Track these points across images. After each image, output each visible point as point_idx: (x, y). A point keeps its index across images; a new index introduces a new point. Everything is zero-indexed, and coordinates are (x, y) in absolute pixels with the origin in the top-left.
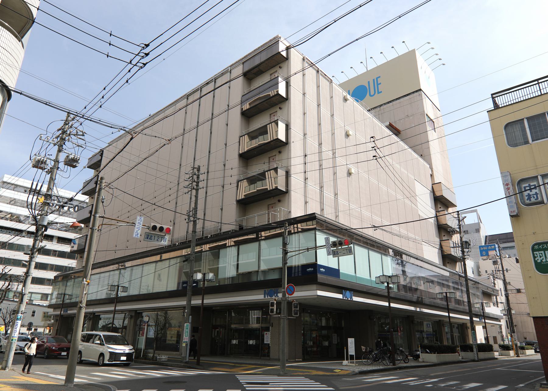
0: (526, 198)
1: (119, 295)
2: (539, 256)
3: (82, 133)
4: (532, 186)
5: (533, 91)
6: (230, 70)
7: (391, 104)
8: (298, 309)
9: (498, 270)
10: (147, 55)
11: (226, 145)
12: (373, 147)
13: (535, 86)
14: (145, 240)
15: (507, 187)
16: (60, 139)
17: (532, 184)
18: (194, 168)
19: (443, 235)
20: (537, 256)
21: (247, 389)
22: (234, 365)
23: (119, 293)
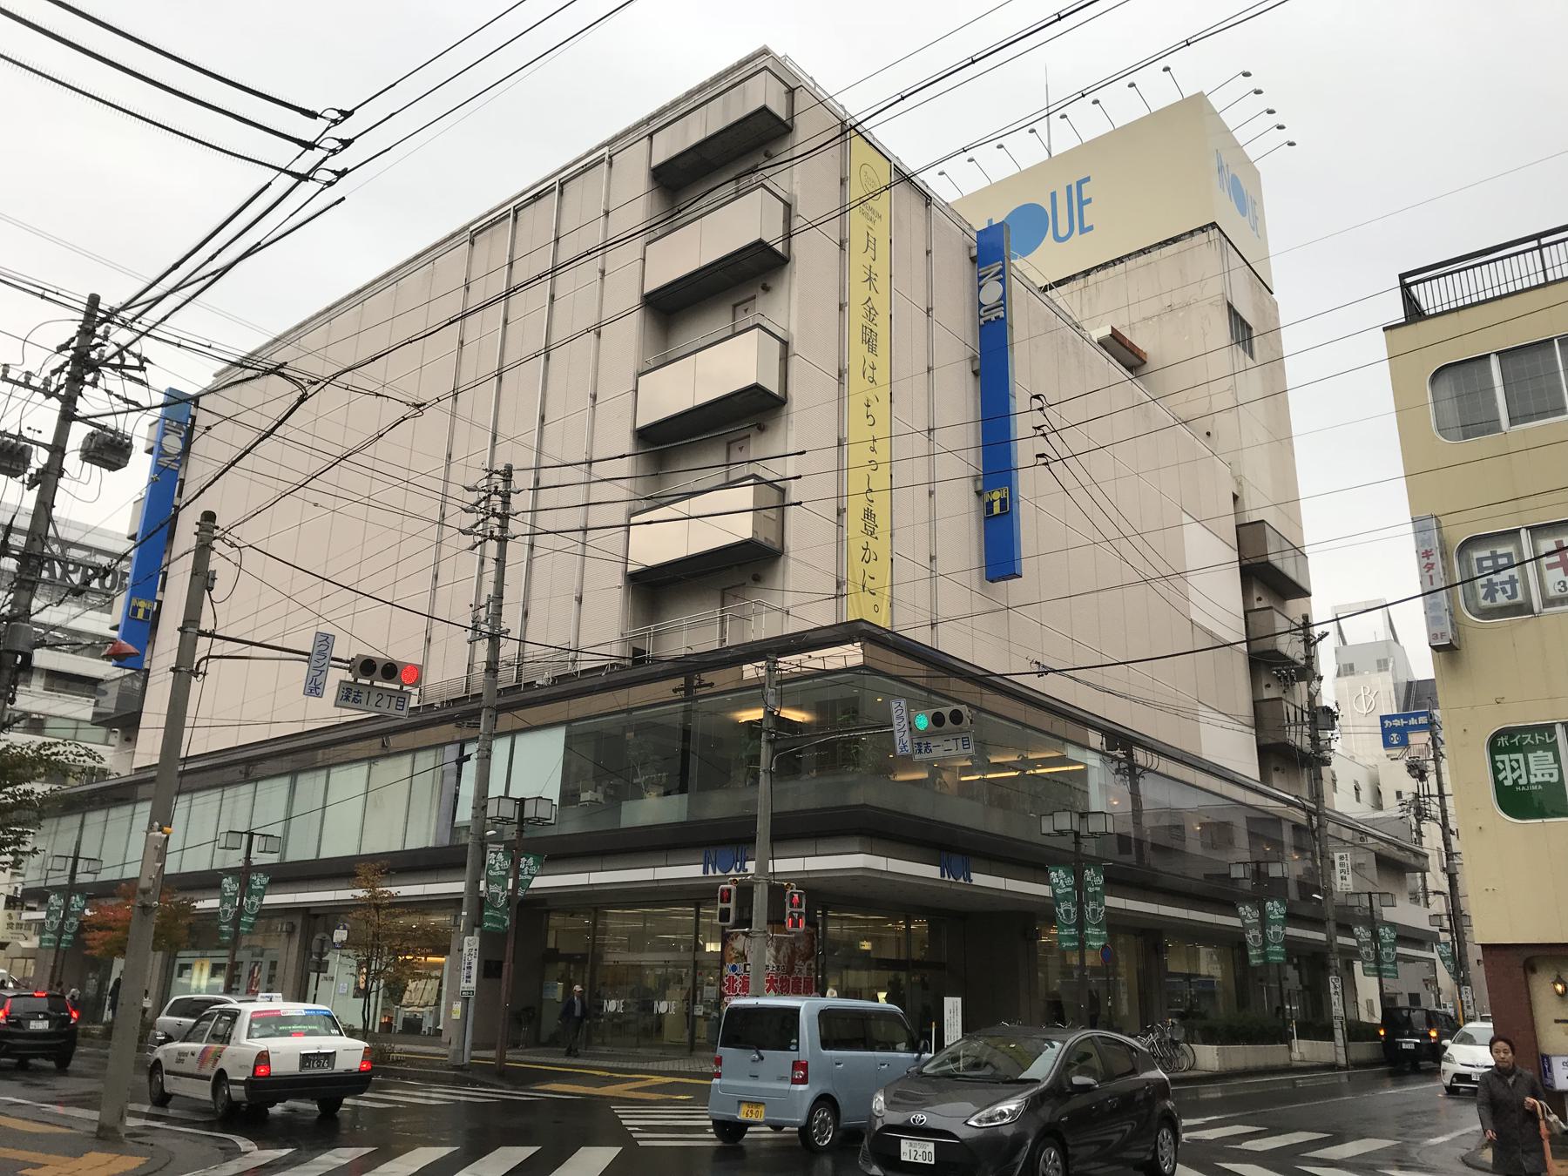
0: (1482, 592)
1: (255, 862)
2: (1508, 768)
3: (136, 363)
4: (1502, 556)
5: (1522, 270)
6: (610, 157)
7: (1120, 267)
8: (803, 910)
9: (1426, 793)
10: (346, 143)
11: (594, 397)
12: (1039, 428)
13: (1528, 255)
14: (339, 703)
15: (1425, 561)
16: (66, 379)
17: (1500, 551)
18: (491, 472)
19: (1264, 682)
20: (1505, 769)
21: (641, 1143)
22: (608, 1074)
23: (254, 853)
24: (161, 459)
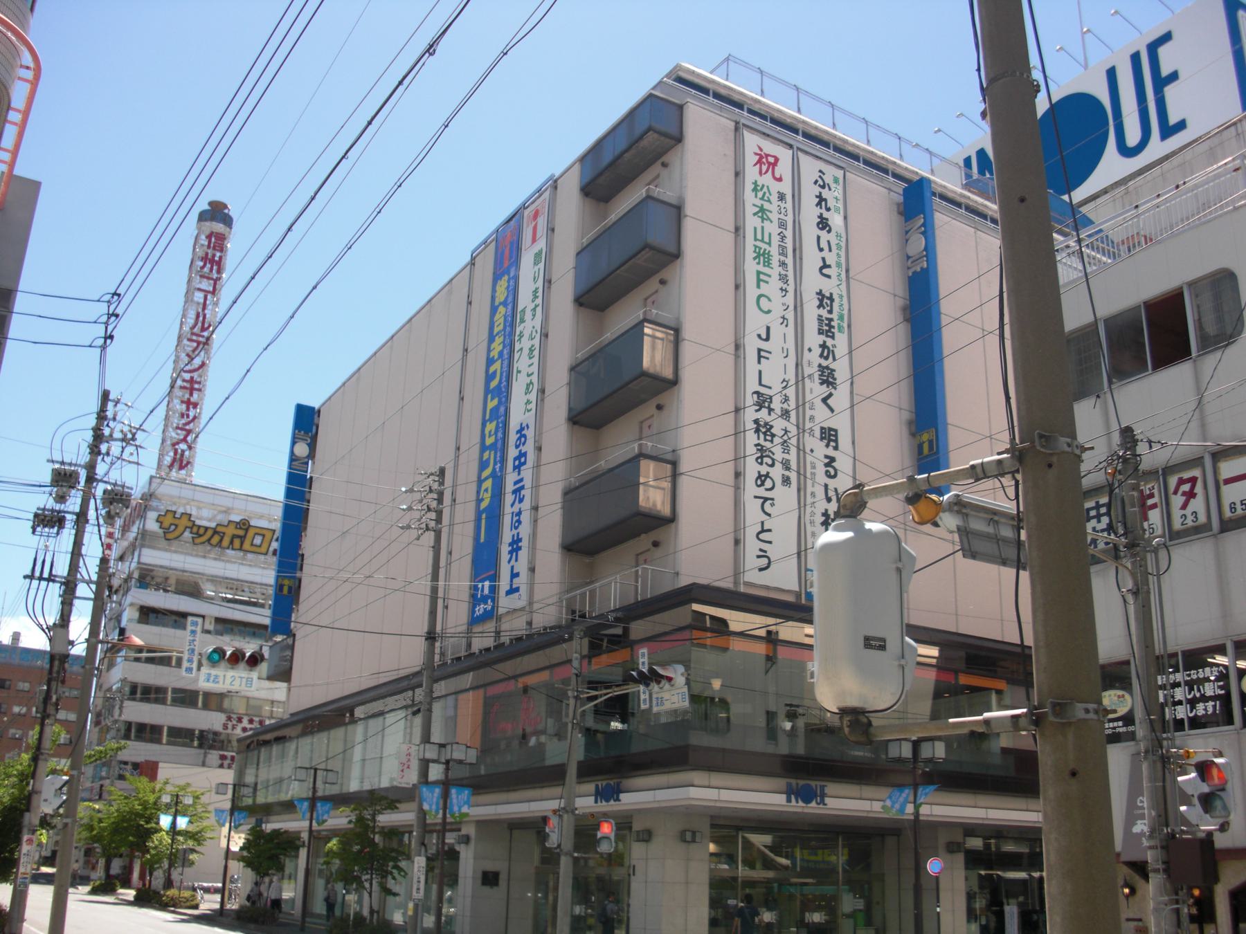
24: (294, 463)
